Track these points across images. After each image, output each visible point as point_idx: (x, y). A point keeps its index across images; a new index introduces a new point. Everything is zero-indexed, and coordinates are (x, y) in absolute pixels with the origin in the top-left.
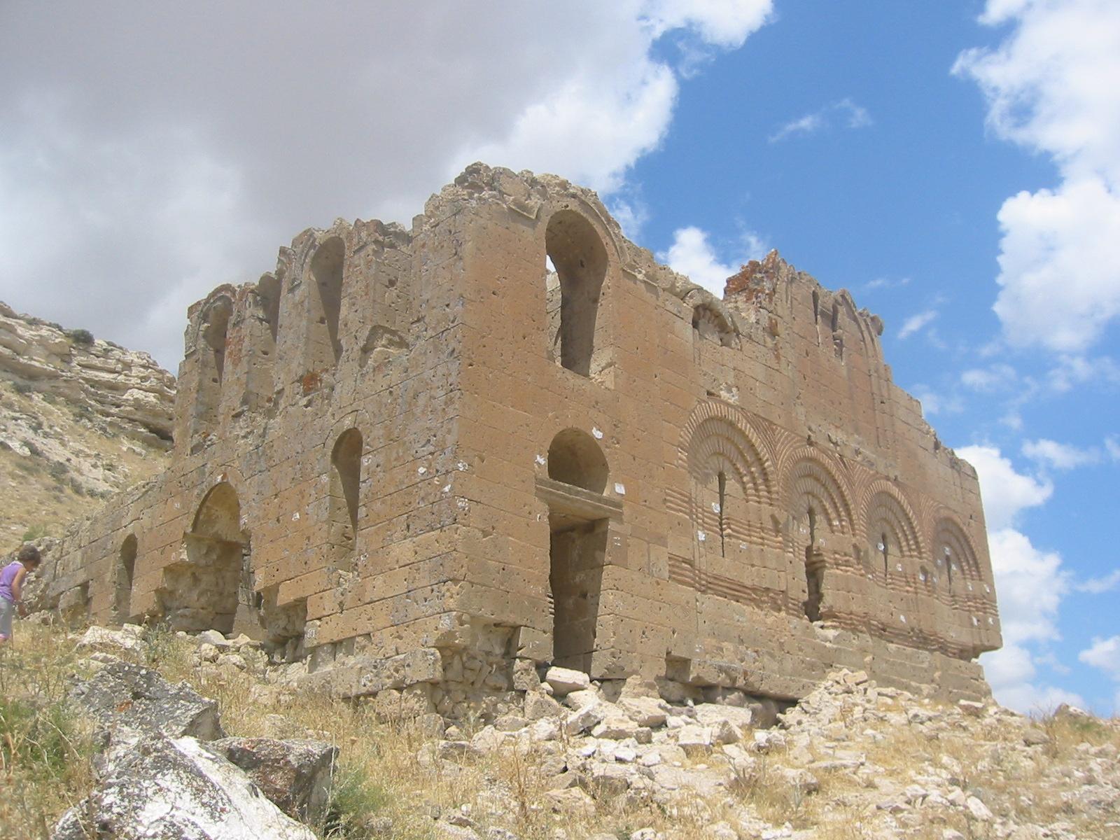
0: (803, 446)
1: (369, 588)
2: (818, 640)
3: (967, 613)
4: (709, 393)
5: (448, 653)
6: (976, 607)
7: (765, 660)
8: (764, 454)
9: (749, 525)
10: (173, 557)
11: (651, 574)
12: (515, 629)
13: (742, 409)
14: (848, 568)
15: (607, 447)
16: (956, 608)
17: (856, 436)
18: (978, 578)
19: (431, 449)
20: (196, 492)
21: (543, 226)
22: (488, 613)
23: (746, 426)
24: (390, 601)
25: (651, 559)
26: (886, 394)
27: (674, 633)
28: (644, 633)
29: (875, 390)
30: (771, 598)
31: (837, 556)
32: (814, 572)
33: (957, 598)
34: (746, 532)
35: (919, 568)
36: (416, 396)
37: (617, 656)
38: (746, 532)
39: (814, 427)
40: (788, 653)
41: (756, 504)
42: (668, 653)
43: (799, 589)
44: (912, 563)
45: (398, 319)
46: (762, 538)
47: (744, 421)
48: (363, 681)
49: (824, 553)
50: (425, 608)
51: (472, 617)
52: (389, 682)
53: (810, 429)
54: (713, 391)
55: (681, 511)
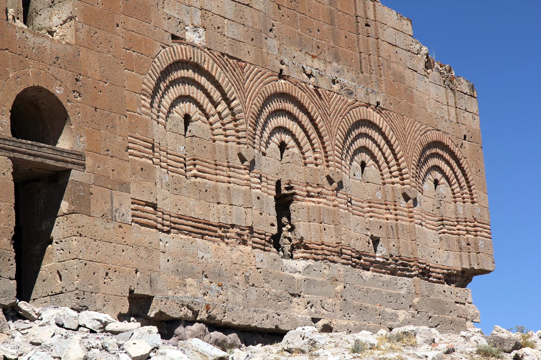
0: (273, 80)
2: (287, 273)
3: (457, 236)
4: (174, 37)
6: (467, 230)
7: (229, 293)
8: (231, 91)
9: (216, 165)
11: (114, 219)
13: (209, 49)
14: (321, 200)
15: (68, 101)
16: (444, 233)
17: (335, 64)
18: (470, 200)
23: (213, 67)
25: (114, 205)
27: (136, 273)
28: (107, 274)
29: (360, 12)
30: (246, 235)
31: (309, 188)
32: (283, 203)
33: (445, 222)
34: (212, 171)
35: (400, 195)
37: (81, 297)
38: (212, 171)
39: (286, 61)
40: (253, 285)
41: (223, 143)
42: (131, 292)
43: (266, 221)
44: (393, 189)
46: (229, 177)
47: (211, 61)
49: (296, 186)
53: (282, 63)
54: (178, 34)
55: (144, 157)
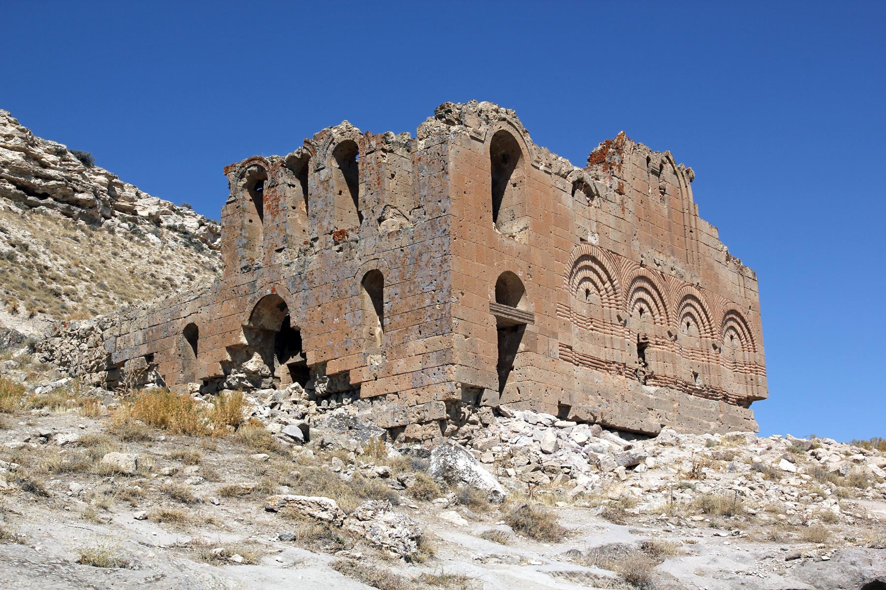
1: (395, 366)
4: (582, 240)
5: (449, 404)
10: (233, 341)
12: (482, 390)
19: (434, 288)
20: (249, 298)
21: (488, 144)
22: (469, 382)
24: (410, 375)
26: (694, 226)
29: (687, 223)
36: (421, 254)
39: (645, 255)
42: (559, 402)
44: (707, 341)
45: (398, 199)
48: (396, 419)
50: (433, 379)
51: (462, 384)
52: (415, 420)
53: (642, 256)
